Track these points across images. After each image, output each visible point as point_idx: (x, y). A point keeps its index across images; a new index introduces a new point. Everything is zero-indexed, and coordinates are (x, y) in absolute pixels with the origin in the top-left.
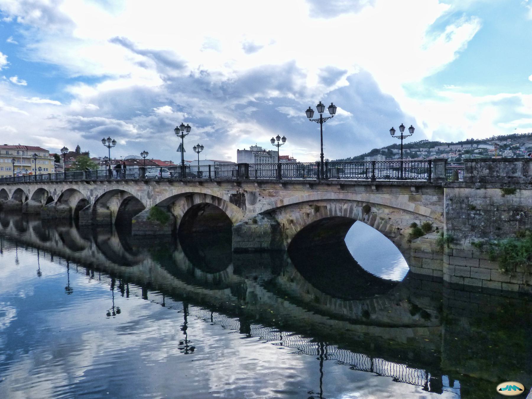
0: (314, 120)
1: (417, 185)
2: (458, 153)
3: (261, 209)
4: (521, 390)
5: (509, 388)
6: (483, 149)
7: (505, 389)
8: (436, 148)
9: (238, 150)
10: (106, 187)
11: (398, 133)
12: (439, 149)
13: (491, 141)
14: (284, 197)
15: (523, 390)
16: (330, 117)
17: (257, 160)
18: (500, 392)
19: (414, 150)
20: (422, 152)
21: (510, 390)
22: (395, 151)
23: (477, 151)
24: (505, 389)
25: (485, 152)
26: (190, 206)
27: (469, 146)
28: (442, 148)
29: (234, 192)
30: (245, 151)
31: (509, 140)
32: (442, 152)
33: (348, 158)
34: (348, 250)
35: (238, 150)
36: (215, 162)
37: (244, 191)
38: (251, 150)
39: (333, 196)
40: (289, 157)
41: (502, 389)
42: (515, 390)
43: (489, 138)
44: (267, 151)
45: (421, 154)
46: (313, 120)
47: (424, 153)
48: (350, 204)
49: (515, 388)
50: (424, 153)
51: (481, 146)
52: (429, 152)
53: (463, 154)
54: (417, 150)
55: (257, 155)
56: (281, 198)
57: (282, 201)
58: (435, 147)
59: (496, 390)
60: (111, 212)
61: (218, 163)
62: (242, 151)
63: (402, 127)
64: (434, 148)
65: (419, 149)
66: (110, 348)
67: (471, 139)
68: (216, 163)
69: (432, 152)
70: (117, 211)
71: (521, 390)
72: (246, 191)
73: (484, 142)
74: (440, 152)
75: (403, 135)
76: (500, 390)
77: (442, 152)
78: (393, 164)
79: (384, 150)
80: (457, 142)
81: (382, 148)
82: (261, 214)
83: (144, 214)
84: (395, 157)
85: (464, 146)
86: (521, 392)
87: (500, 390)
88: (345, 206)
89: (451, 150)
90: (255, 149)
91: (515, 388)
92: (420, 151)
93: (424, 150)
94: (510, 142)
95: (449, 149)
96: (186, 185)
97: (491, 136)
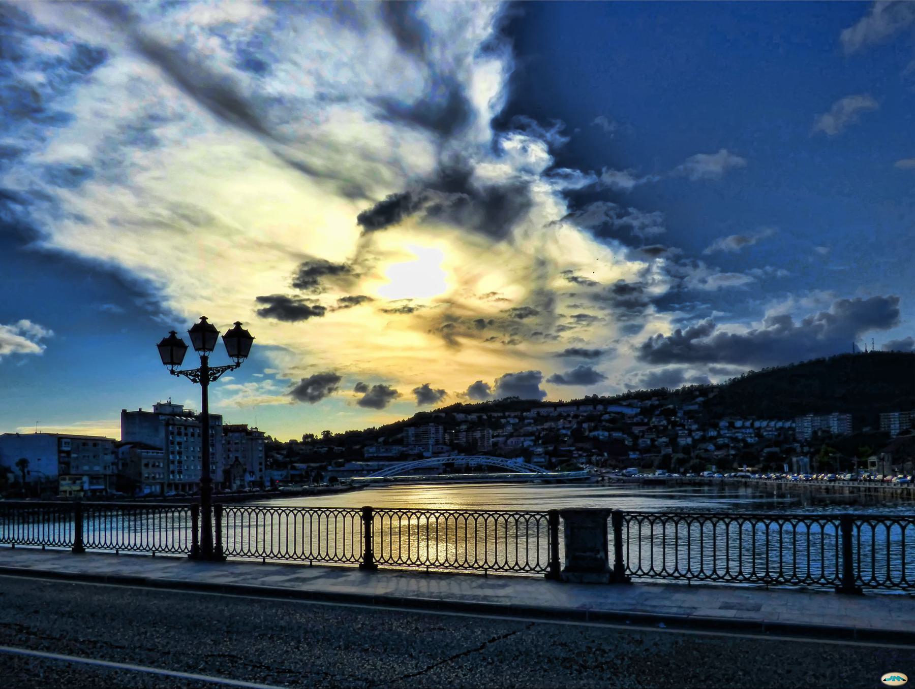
0: (186, 373)
4: (904, 680)
5: (893, 679)
6: (615, 413)
7: (889, 679)
8: (533, 413)
9: (124, 412)
12: (538, 413)
16: (229, 367)
18: (885, 682)
19: (495, 415)
20: (509, 419)
22: (460, 416)
23: (607, 417)
24: (889, 679)
27: (591, 408)
28: (543, 411)
30: (141, 414)
31: (654, 398)
35: (124, 412)
38: (158, 412)
40: (249, 428)
45: (508, 422)
46: (181, 372)
47: (512, 421)
49: (899, 679)
50: (512, 421)
51: (612, 409)
53: (583, 422)
54: (500, 414)
59: (880, 681)
61: (69, 440)
62: (132, 415)
64: (529, 410)
66: (704, 496)
67: (591, 396)
71: (904, 680)
74: (540, 419)
76: (885, 680)
77: (547, 418)
78: (179, 512)
80: (569, 401)
84: (461, 427)
85: (581, 408)
86: (904, 682)
87: (885, 680)
91: (899, 679)
92: (504, 417)
93: (513, 414)
94: (657, 402)
95: (555, 414)
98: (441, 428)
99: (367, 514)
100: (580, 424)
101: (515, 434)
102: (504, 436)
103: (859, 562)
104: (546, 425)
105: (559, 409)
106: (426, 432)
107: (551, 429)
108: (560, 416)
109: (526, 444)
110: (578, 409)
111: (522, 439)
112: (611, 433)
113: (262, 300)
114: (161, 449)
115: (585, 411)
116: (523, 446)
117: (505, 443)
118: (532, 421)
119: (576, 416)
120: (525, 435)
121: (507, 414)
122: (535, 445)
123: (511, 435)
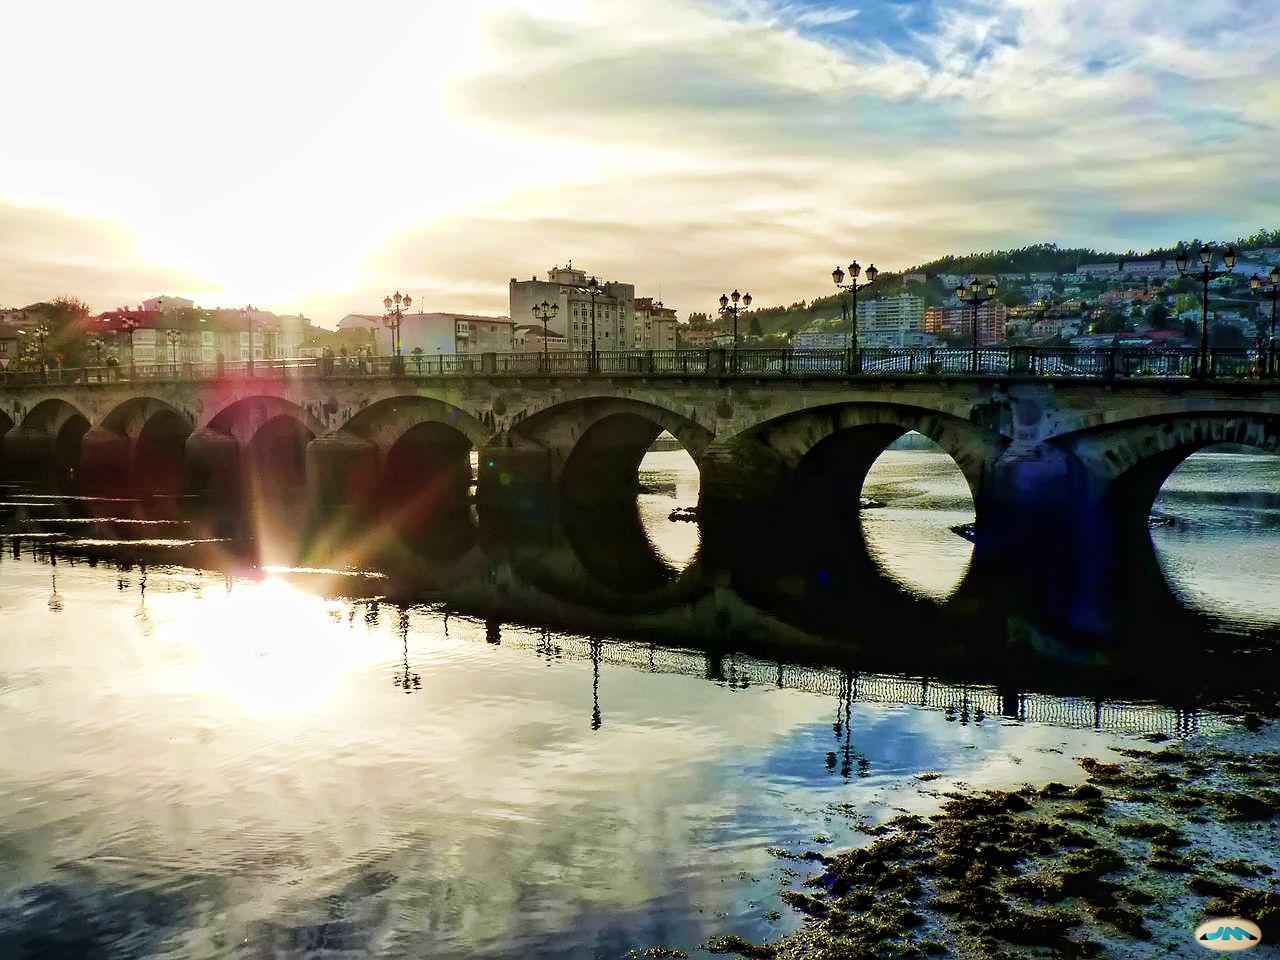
1: (1228, 383)
2: (1154, 291)
3: (1051, 432)
4: (1252, 938)
5: (1224, 934)
7: (1216, 936)
9: (514, 281)
10: (558, 393)
11: (543, 357)
13: (1253, 249)
14: (1106, 409)
15: (1259, 940)
17: (576, 313)
21: (1228, 939)
22: (950, 280)
24: (1216, 936)
25: (1238, 287)
26: (831, 431)
29: (981, 401)
32: (1102, 286)
33: (795, 305)
34: (973, 556)
35: (514, 281)
36: (457, 320)
37: (1011, 398)
38: (554, 281)
39: (1213, 407)
41: (1207, 936)
42: (1240, 939)
43: (1247, 239)
44: (602, 282)
48: (1240, 421)
49: (1239, 933)
52: (1059, 286)
53: (1170, 292)
55: (575, 297)
56: (1098, 411)
57: (1101, 416)
58: (1079, 270)
60: (550, 451)
61: (467, 323)
62: (525, 285)
63: (855, 268)
65: (1028, 276)
67: (1190, 242)
68: (460, 323)
69: (1069, 284)
70: (571, 449)
71: (1252, 938)
72: (1016, 400)
73: (1232, 252)
74: (1094, 286)
75: (857, 283)
76: (1204, 938)
77: (1102, 286)
79: (915, 277)
81: (908, 272)
82: (1046, 441)
83: (1164, 425)
87: (1204, 938)
88: (1230, 424)
89: (1130, 277)
90: (565, 280)
91: (1239, 933)
93: (1045, 277)
96: (65, 391)
97: (1256, 234)
98: (920, 301)
99: (429, 363)
100: (1163, 295)
101: (1045, 315)
102: (1026, 318)
103: (950, 356)
104: (1102, 298)
105: (1128, 268)
106: (895, 310)
107: (1110, 306)
108: (1128, 283)
109: (1064, 333)
110: (1163, 266)
111: (1059, 323)
112: (1219, 313)
113: (539, 35)
114: (561, 336)
115: (1172, 271)
116: (1059, 335)
117: (1029, 330)
118: (1078, 289)
119: (1158, 282)
120: (1063, 317)
121: (1034, 276)
122: (1080, 334)
123: (1039, 316)
